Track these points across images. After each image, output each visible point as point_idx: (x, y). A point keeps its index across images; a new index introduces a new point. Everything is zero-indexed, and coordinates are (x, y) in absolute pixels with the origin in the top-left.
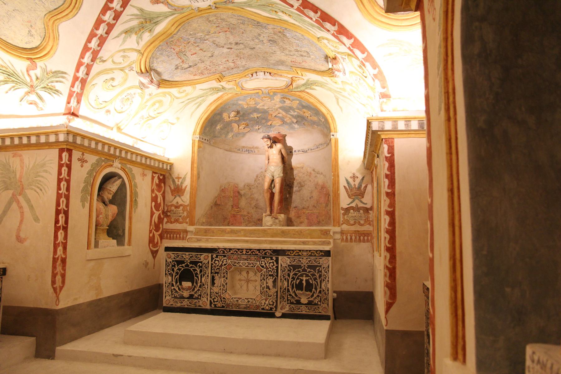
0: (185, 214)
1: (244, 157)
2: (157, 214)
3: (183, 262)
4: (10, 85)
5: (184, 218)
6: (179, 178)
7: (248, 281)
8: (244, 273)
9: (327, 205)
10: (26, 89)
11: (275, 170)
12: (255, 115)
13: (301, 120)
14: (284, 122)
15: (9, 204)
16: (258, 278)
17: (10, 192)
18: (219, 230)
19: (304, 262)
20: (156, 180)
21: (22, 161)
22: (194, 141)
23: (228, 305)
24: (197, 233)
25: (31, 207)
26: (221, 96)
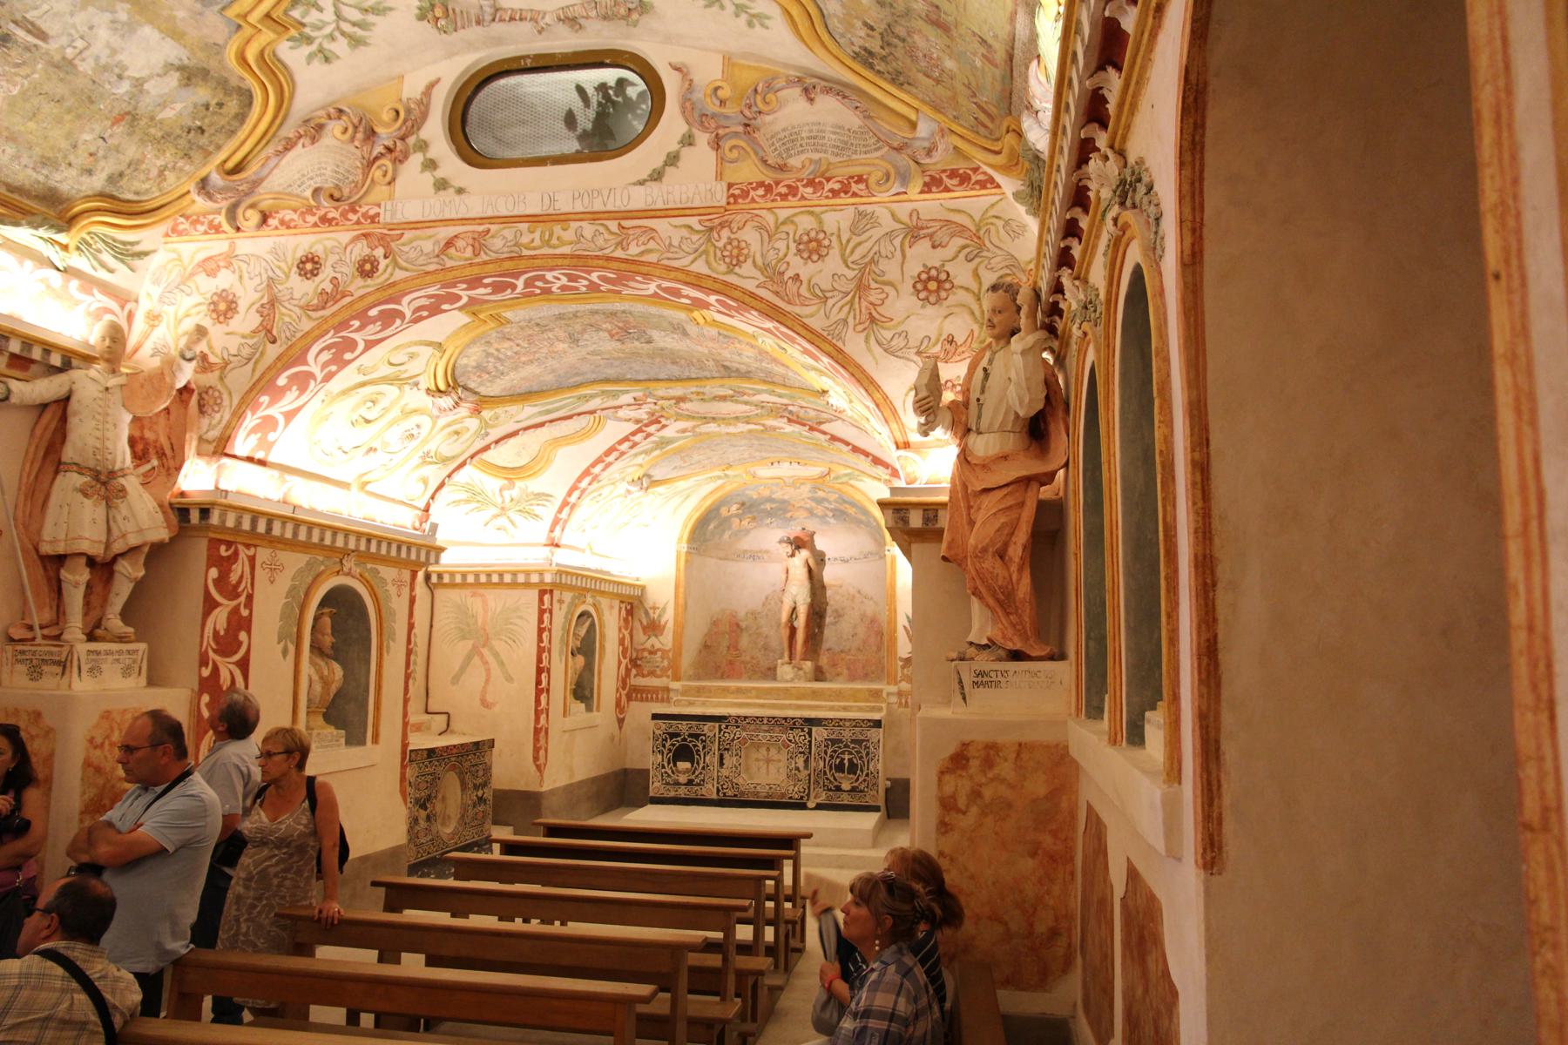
0: (666, 663)
1: (746, 567)
2: (624, 662)
3: (678, 735)
4: (474, 505)
5: (664, 670)
6: (654, 608)
7: (768, 761)
8: (763, 751)
9: (879, 649)
10: (496, 511)
11: (799, 593)
12: (768, 506)
13: (840, 514)
14: (811, 513)
15: (469, 658)
16: (784, 755)
17: (470, 643)
18: (719, 688)
19: (847, 735)
20: (624, 613)
21: (485, 603)
22: (679, 553)
23: (743, 793)
24: (685, 692)
25: (501, 663)
26: (722, 487)
